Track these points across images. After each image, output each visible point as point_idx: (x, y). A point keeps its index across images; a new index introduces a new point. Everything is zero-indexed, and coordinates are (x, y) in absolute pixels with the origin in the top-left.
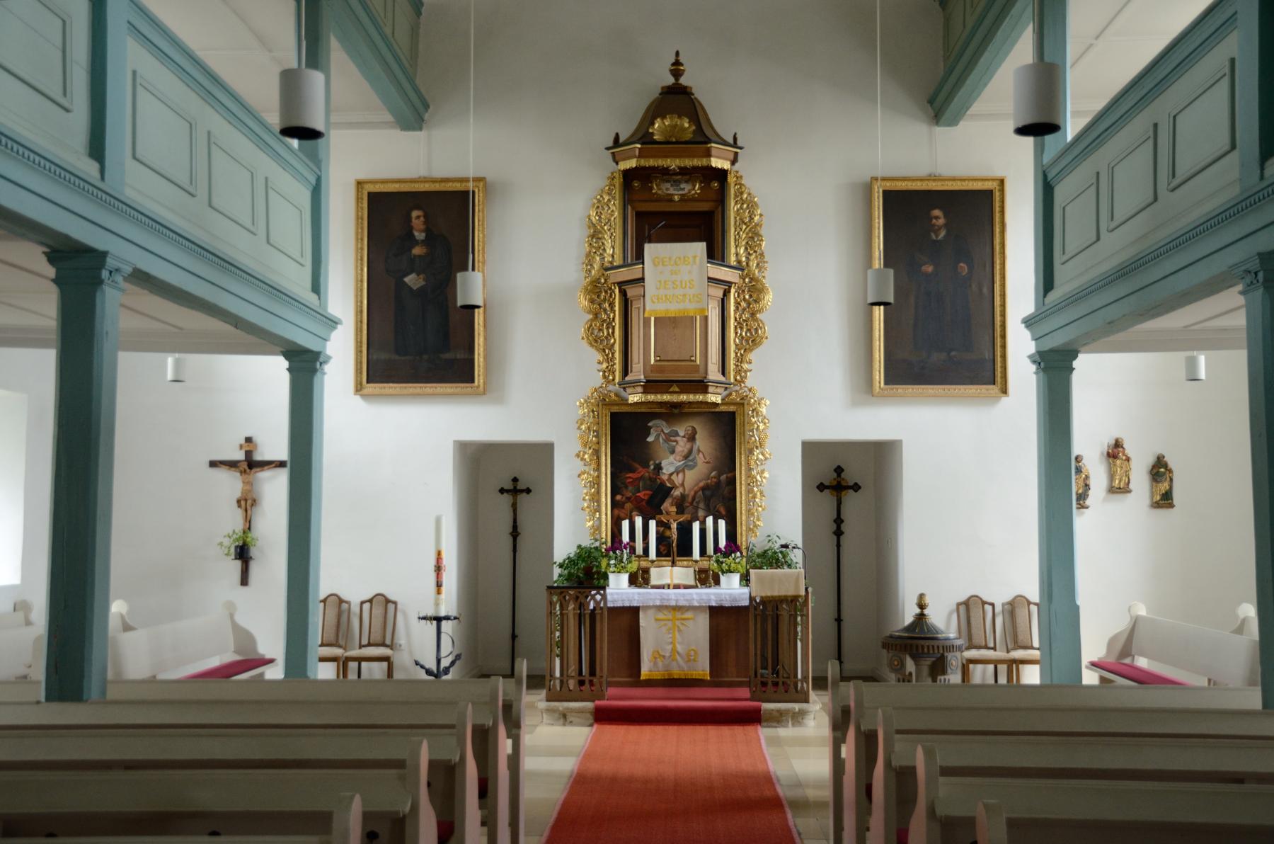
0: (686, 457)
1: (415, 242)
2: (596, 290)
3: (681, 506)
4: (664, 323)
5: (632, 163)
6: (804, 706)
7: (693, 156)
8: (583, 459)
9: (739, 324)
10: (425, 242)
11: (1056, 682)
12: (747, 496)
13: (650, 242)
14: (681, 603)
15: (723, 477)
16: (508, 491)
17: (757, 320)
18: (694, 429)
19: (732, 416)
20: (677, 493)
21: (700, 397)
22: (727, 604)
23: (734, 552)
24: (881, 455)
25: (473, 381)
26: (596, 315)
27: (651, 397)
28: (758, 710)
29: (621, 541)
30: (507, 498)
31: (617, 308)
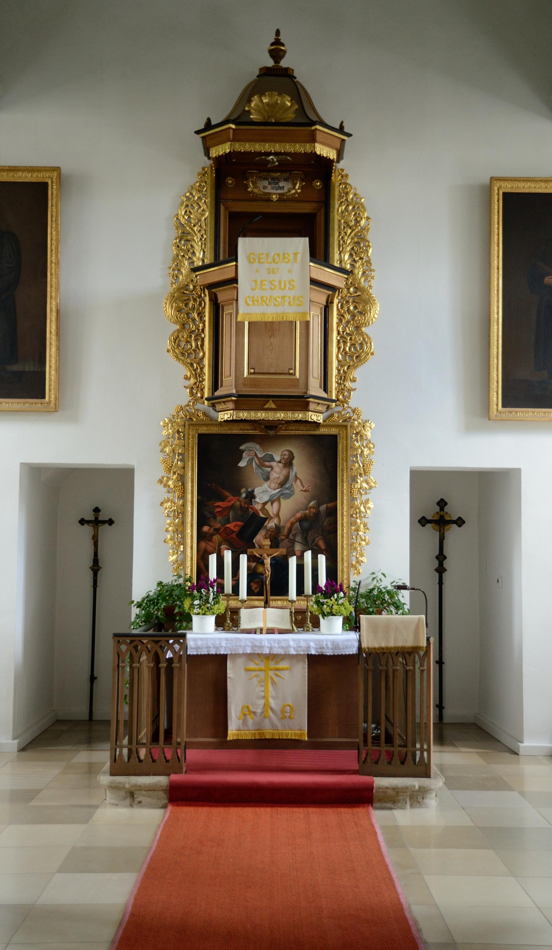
0: (282, 485)
2: (182, 298)
3: (275, 538)
4: (262, 329)
5: (224, 149)
6: (424, 782)
7: (294, 140)
8: (166, 485)
9: (342, 339)
12: (349, 529)
13: (245, 236)
14: (276, 651)
15: (323, 508)
16: (88, 522)
17: (362, 334)
18: (291, 453)
19: (334, 439)
20: (271, 524)
21: (299, 416)
22: (329, 652)
23: (337, 592)
24: (493, 487)
25: (44, 397)
26: (183, 326)
27: (244, 415)
28: (369, 788)
29: (207, 578)
30: (88, 530)
31: (207, 319)
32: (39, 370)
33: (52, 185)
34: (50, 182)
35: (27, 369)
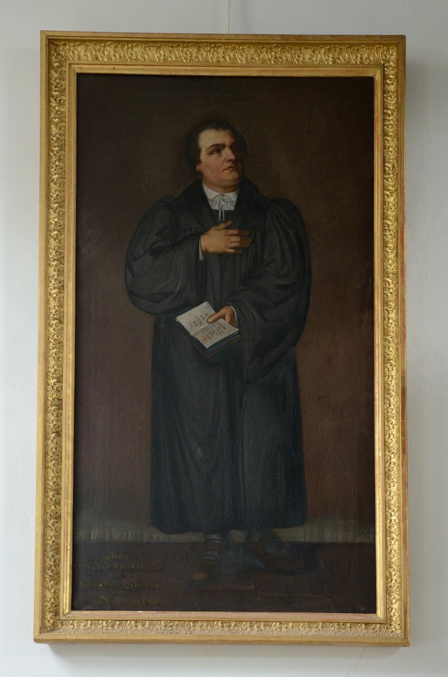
1: (208, 218)
10: (236, 219)
11: (230, 33)
32: (358, 540)
33: (384, 84)
34: (378, 78)
35: (329, 536)
